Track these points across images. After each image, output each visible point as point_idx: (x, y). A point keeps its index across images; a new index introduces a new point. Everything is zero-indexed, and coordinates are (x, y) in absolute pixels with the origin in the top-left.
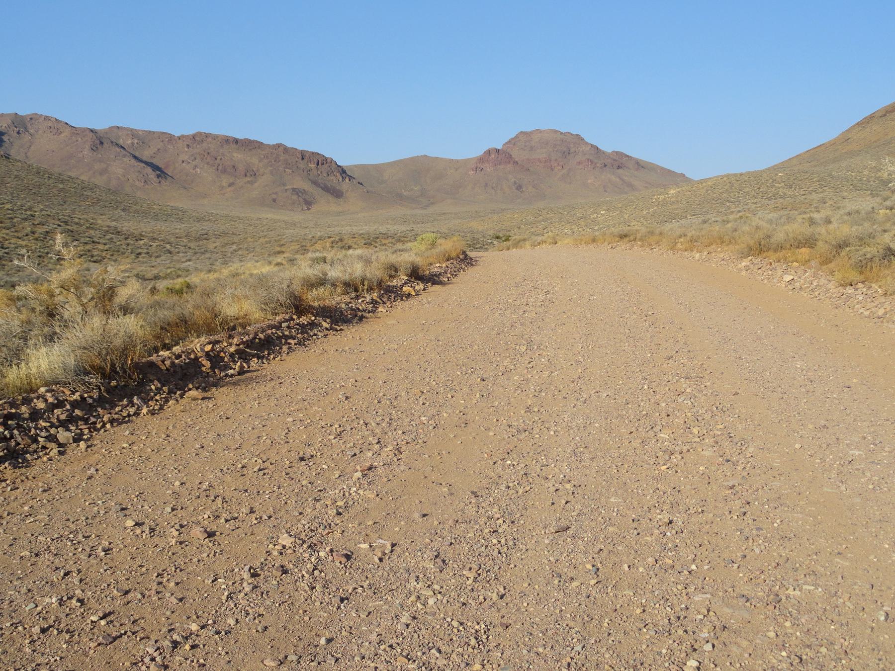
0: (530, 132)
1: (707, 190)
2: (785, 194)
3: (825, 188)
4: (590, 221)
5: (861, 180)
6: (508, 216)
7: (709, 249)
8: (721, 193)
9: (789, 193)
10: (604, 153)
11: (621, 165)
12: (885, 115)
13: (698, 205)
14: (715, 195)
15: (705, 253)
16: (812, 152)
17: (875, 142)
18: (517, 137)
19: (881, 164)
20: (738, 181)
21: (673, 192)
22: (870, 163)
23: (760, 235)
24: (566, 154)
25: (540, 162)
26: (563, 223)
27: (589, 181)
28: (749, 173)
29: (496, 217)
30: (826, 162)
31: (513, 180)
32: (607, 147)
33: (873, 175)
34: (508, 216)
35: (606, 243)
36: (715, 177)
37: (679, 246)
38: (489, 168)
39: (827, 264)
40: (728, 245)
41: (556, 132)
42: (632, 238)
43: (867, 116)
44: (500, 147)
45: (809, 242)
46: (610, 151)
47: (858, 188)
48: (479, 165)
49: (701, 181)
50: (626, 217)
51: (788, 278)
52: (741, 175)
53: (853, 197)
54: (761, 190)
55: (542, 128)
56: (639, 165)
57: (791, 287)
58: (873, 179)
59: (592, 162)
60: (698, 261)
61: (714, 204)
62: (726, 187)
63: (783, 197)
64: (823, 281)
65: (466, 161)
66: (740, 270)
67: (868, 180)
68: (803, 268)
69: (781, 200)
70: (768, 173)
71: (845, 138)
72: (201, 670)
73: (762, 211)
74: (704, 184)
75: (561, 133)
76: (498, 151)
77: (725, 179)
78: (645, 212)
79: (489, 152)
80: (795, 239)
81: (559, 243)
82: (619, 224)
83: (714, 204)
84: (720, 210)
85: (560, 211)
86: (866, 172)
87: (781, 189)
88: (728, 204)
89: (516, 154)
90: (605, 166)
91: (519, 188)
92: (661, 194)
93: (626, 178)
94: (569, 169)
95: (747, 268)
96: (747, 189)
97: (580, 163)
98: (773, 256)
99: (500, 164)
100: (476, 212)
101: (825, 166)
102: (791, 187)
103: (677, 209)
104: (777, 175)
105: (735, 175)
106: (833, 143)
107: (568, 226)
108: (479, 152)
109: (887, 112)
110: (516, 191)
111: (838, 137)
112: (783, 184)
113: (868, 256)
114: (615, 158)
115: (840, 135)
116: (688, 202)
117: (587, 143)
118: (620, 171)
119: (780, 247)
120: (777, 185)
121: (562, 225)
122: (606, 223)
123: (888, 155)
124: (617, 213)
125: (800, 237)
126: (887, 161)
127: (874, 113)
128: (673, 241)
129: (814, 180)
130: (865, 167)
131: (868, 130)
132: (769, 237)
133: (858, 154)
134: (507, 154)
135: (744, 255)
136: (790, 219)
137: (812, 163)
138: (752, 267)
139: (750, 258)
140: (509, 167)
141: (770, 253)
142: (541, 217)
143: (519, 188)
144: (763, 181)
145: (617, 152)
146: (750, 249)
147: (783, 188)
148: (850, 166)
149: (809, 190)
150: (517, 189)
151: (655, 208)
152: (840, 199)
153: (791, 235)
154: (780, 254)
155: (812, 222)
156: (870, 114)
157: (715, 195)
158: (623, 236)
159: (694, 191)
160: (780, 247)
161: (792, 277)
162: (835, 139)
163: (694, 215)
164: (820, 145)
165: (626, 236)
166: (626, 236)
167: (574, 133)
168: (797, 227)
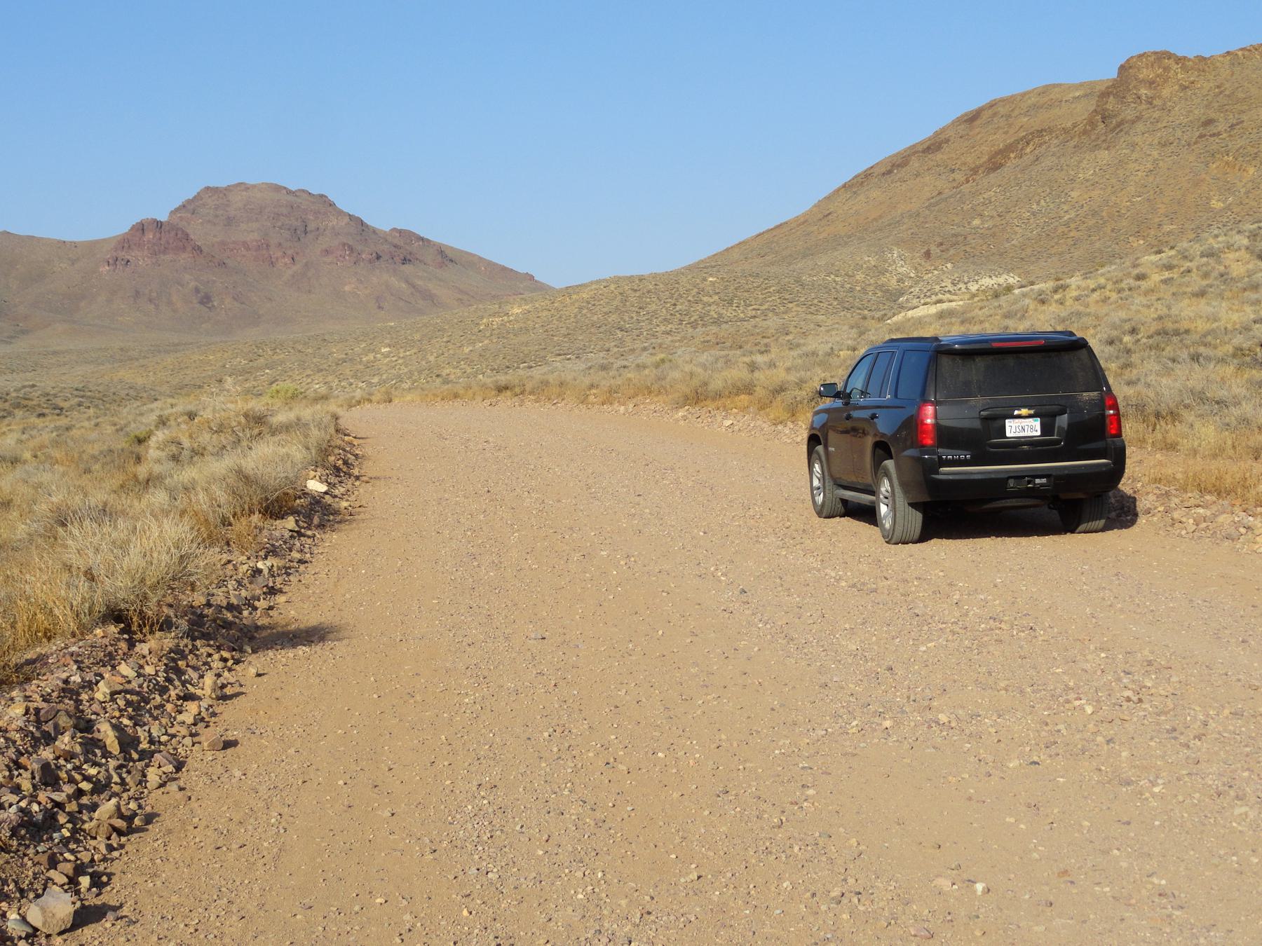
0: (226, 189)
1: (581, 308)
2: (720, 315)
3: (790, 305)
4: (361, 367)
5: (851, 290)
6: (196, 357)
7: (635, 400)
8: (606, 313)
9: (728, 313)
10: (374, 231)
11: (408, 257)
12: (890, 172)
13: (565, 336)
14: (595, 318)
15: (631, 406)
16: (766, 236)
17: (875, 220)
18: (198, 197)
19: (885, 261)
20: (636, 291)
21: (516, 310)
22: (866, 259)
23: (695, 382)
24: (301, 232)
25: (248, 249)
26: (309, 372)
27: (347, 288)
28: (655, 276)
29: (169, 360)
30: (791, 255)
31: (193, 284)
32: (382, 220)
33: (872, 281)
34: (196, 357)
35: (479, 399)
36: (592, 283)
37: (592, 398)
38: (141, 259)
39: (764, 409)
40: (657, 395)
41: (278, 188)
42: (517, 390)
43: (859, 171)
44: (163, 217)
45: (748, 389)
46: (387, 228)
47: (846, 305)
48: (121, 254)
49: (569, 291)
50: (432, 358)
51: (728, 423)
52: (641, 279)
53: (834, 324)
54: (678, 308)
55: (251, 181)
56: (446, 257)
57: (730, 430)
58: (872, 288)
59: (351, 249)
60: (624, 414)
61: (594, 334)
62: (615, 303)
63: (717, 322)
64: (759, 423)
65: (92, 246)
66: (677, 420)
67: (864, 291)
68: (742, 413)
69: (714, 329)
70: (689, 277)
71: (823, 212)
72: (32, 944)
73: (683, 349)
74: (574, 297)
75: (289, 192)
76: (159, 225)
77: (612, 287)
78: (467, 350)
79: (141, 228)
80: (734, 386)
81: (396, 401)
82: (420, 372)
83: (594, 334)
84: (607, 345)
85: (300, 347)
86: (860, 276)
87: (713, 307)
88: (620, 334)
89: (198, 231)
90: (378, 257)
91: (206, 300)
92: (494, 315)
93: (420, 283)
94: (306, 264)
95: (685, 418)
96: (654, 307)
97: (327, 252)
98: (711, 406)
99: (165, 252)
100: (122, 349)
101: (790, 264)
102: (731, 304)
103: (527, 344)
104: (705, 279)
105: (630, 279)
106: (802, 222)
107: (319, 377)
108: (121, 226)
109: (893, 165)
110: (197, 306)
111: (811, 211)
112: (716, 297)
113: (798, 399)
114: (396, 241)
115: (815, 206)
116: (547, 331)
117: (341, 212)
118: (407, 268)
119: (718, 395)
120: (705, 299)
121: (308, 376)
122: (393, 371)
123: (898, 245)
124: (413, 351)
125: (739, 384)
126: (895, 255)
127: (872, 167)
128: (583, 393)
129: (771, 290)
130: (858, 267)
131: (862, 197)
132: (706, 384)
133: (846, 243)
134: (180, 233)
135: (679, 405)
136: (728, 362)
137: (767, 258)
138: (690, 416)
139: (687, 407)
140: (185, 258)
141: (708, 402)
142: (262, 360)
143: (206, 300)
144: (682, 290)
145: (400, 231)
146: (686, 398)
147: (718, 305)
148: (833, 265)
149: (763, 308)
150: (201, 303)
151: (486, 342)
152: (812, 326)
153: (729, 382)
154: (720, 403)
155: (753, 367)
156: (865, 168)
157: (595, 318)
158: (501, 389)
159: (557, 309)
160: (718, 395)
161: (731, 422)
162: (804, 215)
163: (560, 355)
164: (781, 225)
165: (506, 388)
166: (506, 388)
167: (315, 192)
168: (738, 373)
